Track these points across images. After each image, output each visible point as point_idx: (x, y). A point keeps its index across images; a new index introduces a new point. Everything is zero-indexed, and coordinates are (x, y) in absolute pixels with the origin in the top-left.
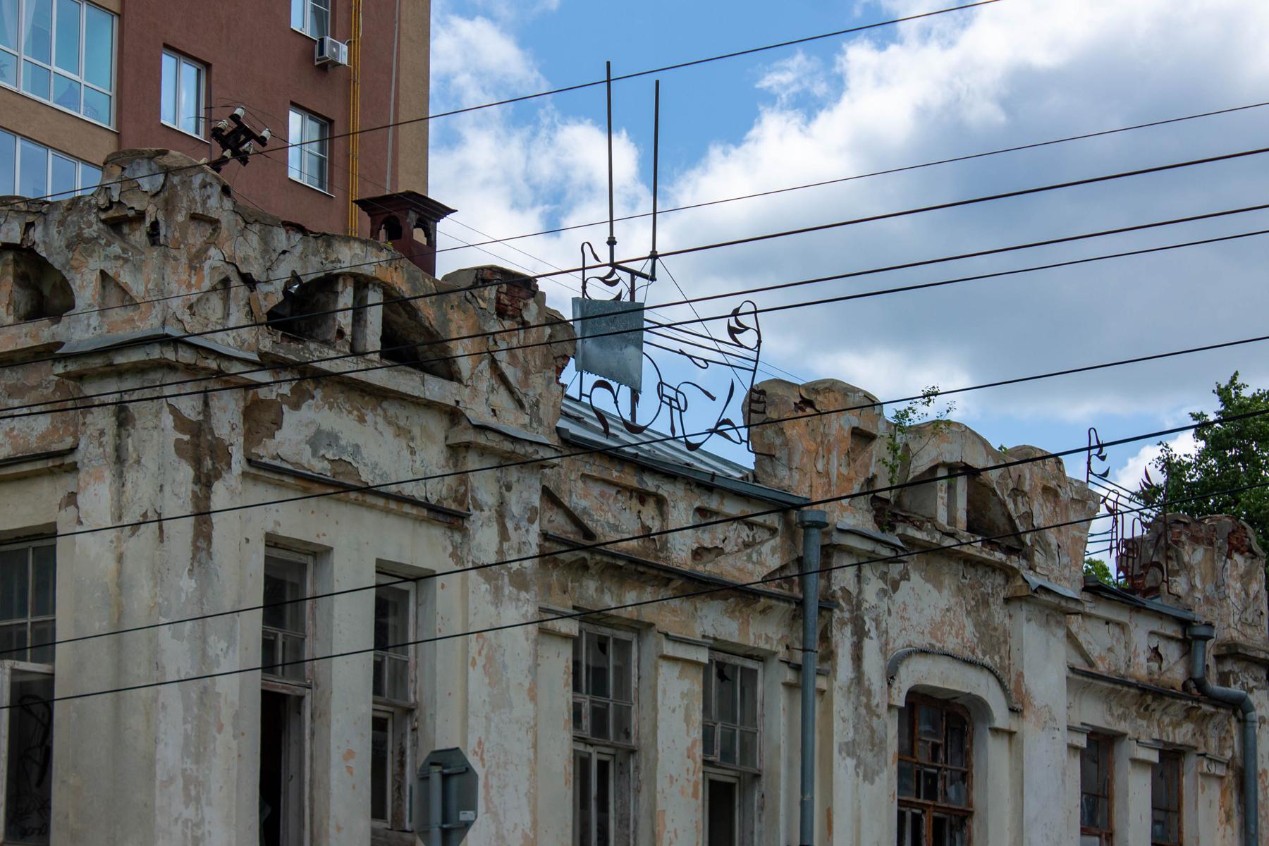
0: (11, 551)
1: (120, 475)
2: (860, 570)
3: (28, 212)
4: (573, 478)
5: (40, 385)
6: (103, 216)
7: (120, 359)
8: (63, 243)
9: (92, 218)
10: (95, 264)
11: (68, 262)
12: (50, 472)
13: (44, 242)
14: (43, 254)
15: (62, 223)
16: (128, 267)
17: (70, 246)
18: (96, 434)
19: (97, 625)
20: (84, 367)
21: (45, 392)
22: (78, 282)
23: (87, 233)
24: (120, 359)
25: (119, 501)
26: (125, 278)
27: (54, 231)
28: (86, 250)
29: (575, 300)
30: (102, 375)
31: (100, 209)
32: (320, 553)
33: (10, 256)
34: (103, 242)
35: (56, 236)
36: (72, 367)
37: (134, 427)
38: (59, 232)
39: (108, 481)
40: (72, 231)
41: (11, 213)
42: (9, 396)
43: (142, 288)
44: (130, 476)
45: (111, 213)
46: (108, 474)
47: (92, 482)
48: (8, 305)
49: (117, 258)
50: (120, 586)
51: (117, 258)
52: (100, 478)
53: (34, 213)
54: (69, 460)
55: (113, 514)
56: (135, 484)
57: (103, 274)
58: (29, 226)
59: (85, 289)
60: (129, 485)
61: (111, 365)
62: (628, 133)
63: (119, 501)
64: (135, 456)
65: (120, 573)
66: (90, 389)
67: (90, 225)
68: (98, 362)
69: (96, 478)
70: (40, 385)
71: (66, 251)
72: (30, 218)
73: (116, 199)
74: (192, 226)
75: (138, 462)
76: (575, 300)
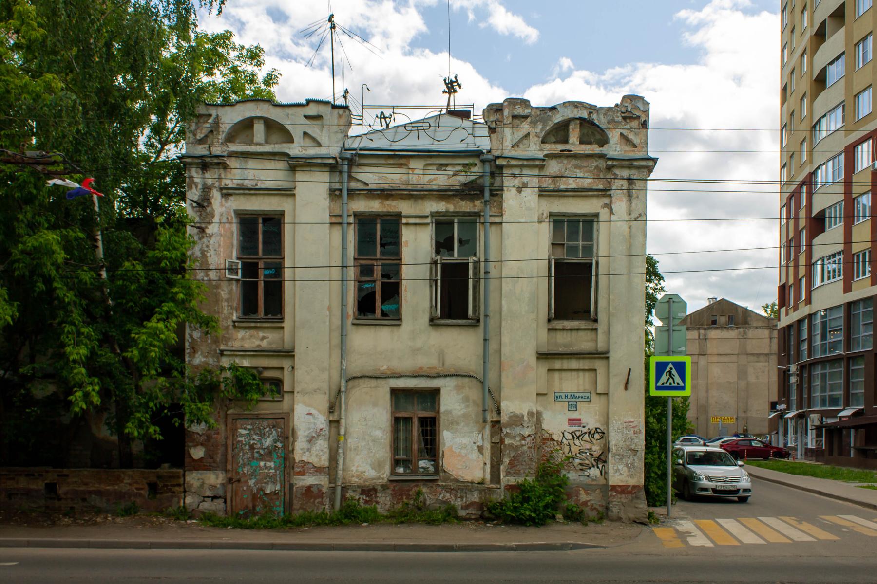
2: (630, 248)
7: (636, 163)
9: (619, 114)
12: (598, 196)
15: (605, 114)
17: (609, 122)
23: (616, 119)
24: (636, 163)
26: (631, 136)
30: (622, 167)
32: (282, 214)
36: (610, 163)
40: (610, 118)
44: (634, 201)
46: (625, 200)
50: (630, 236)
52: (622, 201)
54: (608, 193)
56: (636, 205)
57: (621, 134)
58: (591, 113)
59: (614, 136)
60: (633, 205)
66: (617, 172)
68: (627, 163)
74: (515, 121)
75: (638, 197)
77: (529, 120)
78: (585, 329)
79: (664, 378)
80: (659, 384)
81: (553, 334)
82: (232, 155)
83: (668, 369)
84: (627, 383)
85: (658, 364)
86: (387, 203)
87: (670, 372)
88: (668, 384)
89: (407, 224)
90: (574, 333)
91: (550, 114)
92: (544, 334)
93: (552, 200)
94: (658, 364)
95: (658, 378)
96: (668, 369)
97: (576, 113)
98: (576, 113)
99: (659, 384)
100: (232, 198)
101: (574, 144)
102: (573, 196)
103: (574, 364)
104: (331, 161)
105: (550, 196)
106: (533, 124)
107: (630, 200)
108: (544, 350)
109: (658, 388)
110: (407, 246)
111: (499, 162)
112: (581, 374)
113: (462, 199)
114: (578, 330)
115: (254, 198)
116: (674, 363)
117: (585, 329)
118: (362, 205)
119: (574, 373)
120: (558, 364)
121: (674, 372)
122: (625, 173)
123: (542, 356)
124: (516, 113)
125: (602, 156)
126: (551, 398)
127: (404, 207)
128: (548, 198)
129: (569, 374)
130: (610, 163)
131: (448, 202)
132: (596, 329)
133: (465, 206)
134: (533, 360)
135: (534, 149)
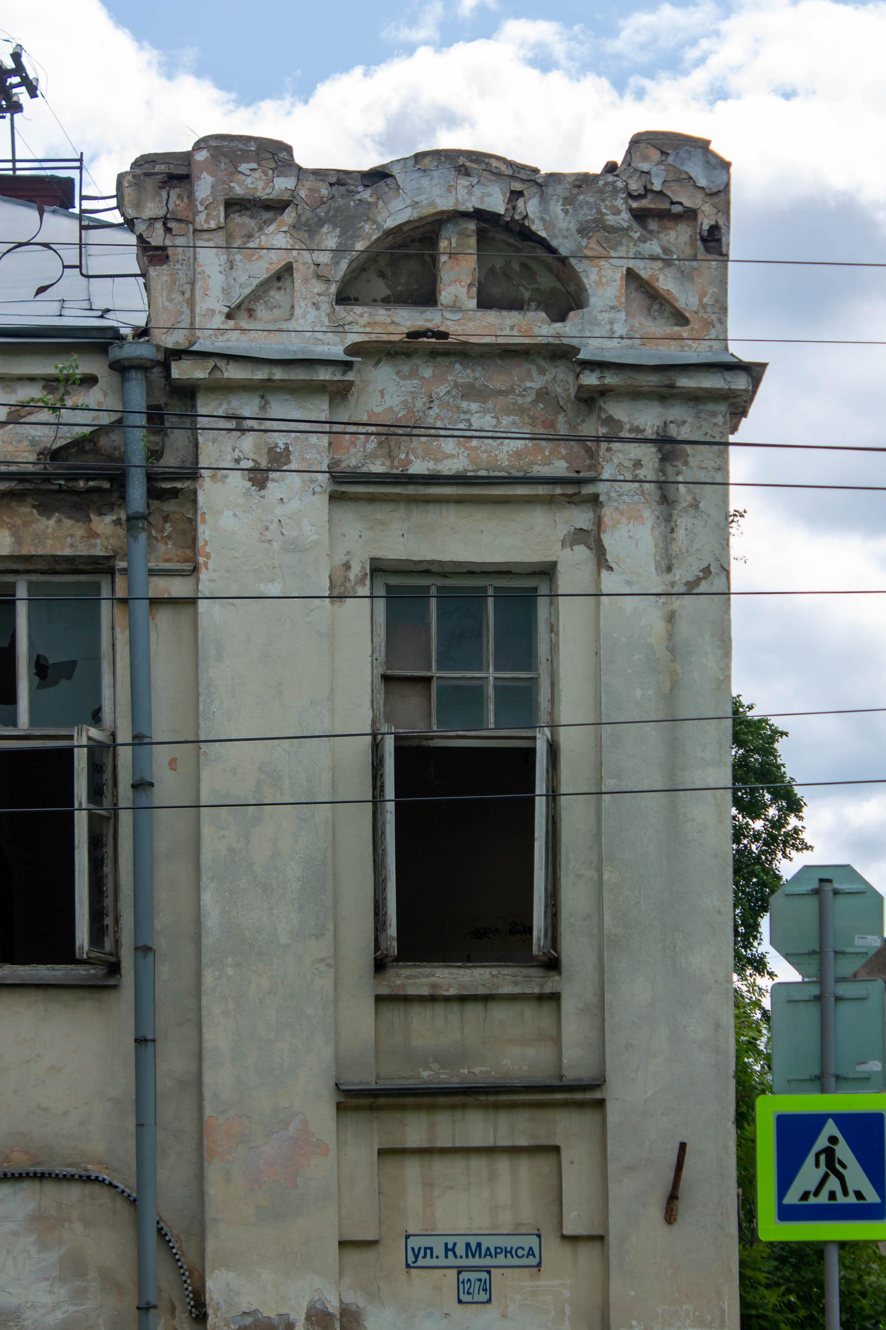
0: (60, 583)
3: (512, 177)
4: (623, 639)
5: (510, 391)
6: (635, 205)
7: (686, 382)
8: (573, 226)
9: (619, 203)
11: (580, 248)
13: (542, 219)
14: (543, 234)
16: (670, 272)
17: (583, 231)
19: (639, 693)
20: (629, 382)
21: (520, 400)
22: (593, 277)
23: (611, 219)
24: (686, 382)
25: (667, 549)
26: (666, 283)
27: (557, 208)
31: (630, 196)
33: (472, 226)
34: (636, 236)
35: (561, 215)
36: (590, 379)
38: (566, 212)
39: (649, 523)
41: (485, 174)
42: (464, 397)
44: (683, 522)
45: (644, 203)
46: (649, 515)
47: (624, 520)
48: (470, 285)
49: (654, 258)
50: (672, 650)
51: (654, 258)
53: (523, 181)
54: (588, 490)
58: (516, 195)
59: (604, 283)
60: (681, 533)
61: (672, 386)
63: (667, 549)
64: (689, 498)
65: (671, 635)
67: (617, 212)
68: (652, 380)
69: (629, 519)
70: (510, 391)
71: (578, 237)
72: (517, 186)
77: (289, 216)
78: (513, 998)
79: (809, 1174)
80: (792, 1198)
81: (395, 1015)
83: (821, 1142)
84: (673, 1197)
85: (785, 1122)
87: (829, 1153)
88: (823, 1198)
90: (473, 1011)
91: (366, 195)
92: (360, 1018)
93: (381, 513)
94: (785, 1122)
95: (784, 1181)
96: (821, 1142)
97: (462, 193)
99: (792, 1198)
102: (460, 501)
103: (476, 1128)
105: (372, 499)
106: (307, 229)
108: (364, 1077)
109: (786, 1213)
111: (180, 371)
112: (503, 1164)
113: (45, 510)
114: (487, 999)
115: (432, 515)
116: (842, 1120)
117: (513, 998)
119: (478, 1163)
120: (415, 1130)
121: (843, 1151)
123: (358, 1100)
124: (239, 191)
126: (394, 1255)
128: (366, 509)
129: (457, 1166)
130: (590, 379)
132: (555, 998)
134: (322, 1115)
135: (309, 326)
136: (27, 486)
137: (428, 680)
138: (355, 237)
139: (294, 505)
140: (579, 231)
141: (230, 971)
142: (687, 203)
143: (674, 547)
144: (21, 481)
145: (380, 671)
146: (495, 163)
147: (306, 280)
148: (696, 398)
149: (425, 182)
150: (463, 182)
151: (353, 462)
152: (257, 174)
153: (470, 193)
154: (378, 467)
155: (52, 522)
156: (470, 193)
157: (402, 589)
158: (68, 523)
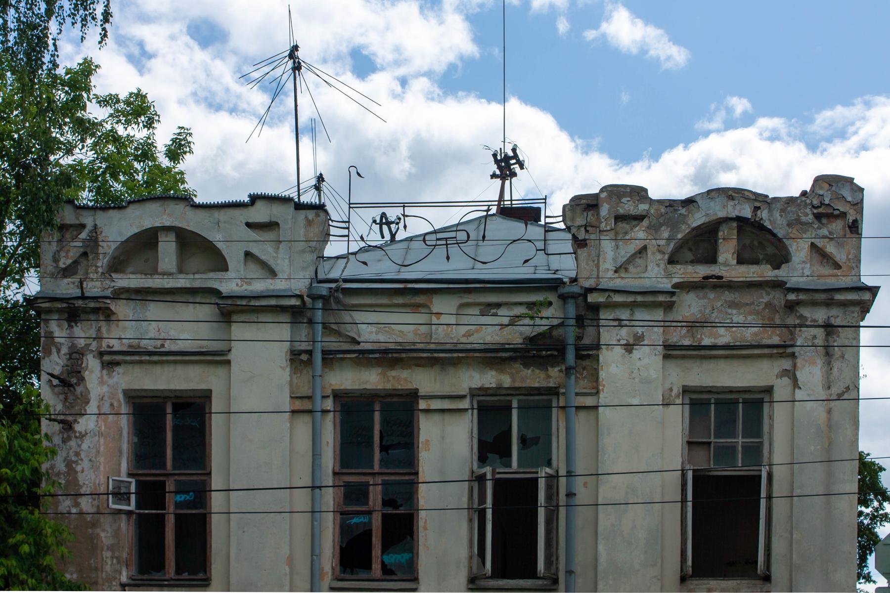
1: (829, 364)
3: (755, 200)
5: (753, 303)
6: (815, 211)
7: (839, 297)
8: (785, 223)
9: (808, 211)
10: (809, 237)
11: (788, 234)
13: (769, 220)
14: (770, 227)
16: (832, 243)
17: (789, 225)
18: (811, 337)
21: (757, 308)
22: (794, 247)
23: (803, 219)
24: (839, 297)
26: (831, 249)
27: (777, 214)
28: (802, 229)
29: (417, 390)
31: (813, 207)
33: (735, 224)
35: (779, 218)
36: (792, 297)
37: (838, 336)
38: (781, 216)
43: (844, 257)
44: (836, 365)
45: (820, 210)
49: (824, 237)
50: (829, 427)
51: (824, 237)
54: (790, 350)
55: (823, 385)
58: (757, 209)
59: (799, 250)
60: (835, 370)
62: (628, 6)
65: (829, 420)
67: (807, 215)
68: (822, 297)
70: (753, 303)
72: (758, 204)
73: (827, 202)
76: (417, 390)
77: (645, 223)
82: (120, 294)
86: (393, 373)
89: (427, 411)
91: (683, 211)
93: (687, 363)
97: (730, 208)
98: (730, 208)
100: (120, 369)
101: (728, 264)
102: (726, 357)
104: (294, 302)
106: (654, 229)
107: (829, 363)
110: (428, 449)
113: (526, 366)
118: (348, 379)
122: (821, 315)
124: (621, 211)
125: (778, 285)
127: (423, 381)
131: (501, 371)
133: (532, 378)
135: (655, 274)
136: (518, 354)
137: (709, 443)
138: (678, 232)
139: (646, 361)
140: (788, 225)
141: (611, 582)
142: (842, 210)
143: (832, 377)
144: (515, 352)
145: (686, 439)
146: (746, 193)
147: (653, 253)
148: (844, 304)
149: (712, 204)
150: (731, 203)
151: (675, 340)
152: (630, 203)
153: (734, 209)
154: (686, 342)
155: (530, 371)
156: (734, 209)
157: (698, 401)
158: (537, 371)
